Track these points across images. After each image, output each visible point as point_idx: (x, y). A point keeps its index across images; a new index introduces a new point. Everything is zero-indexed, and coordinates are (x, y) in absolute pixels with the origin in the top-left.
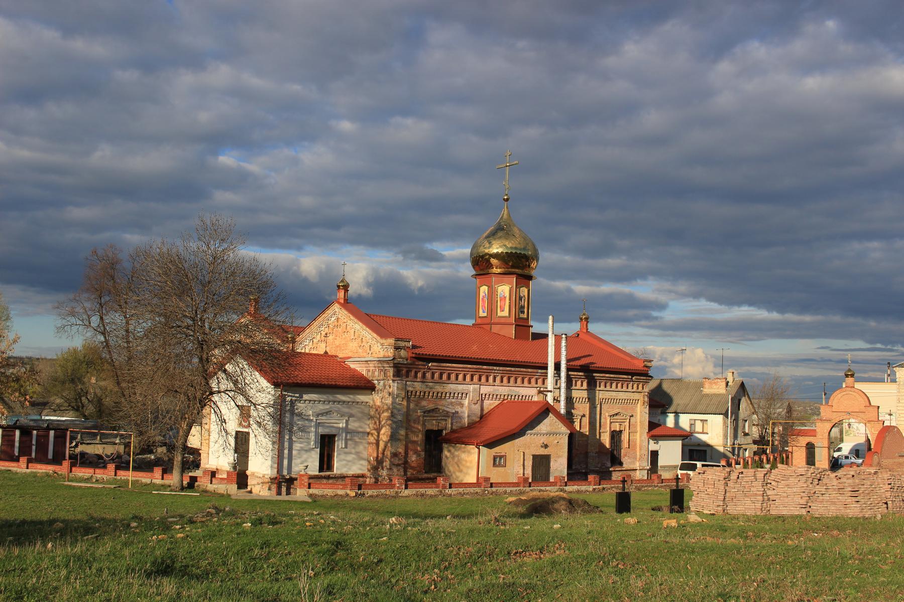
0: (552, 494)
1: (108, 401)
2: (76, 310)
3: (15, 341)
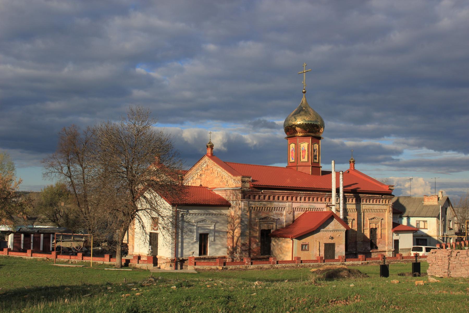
0: (338, 267)
1: (72, 216)
2: (54, 163)
3: (19, 183)
